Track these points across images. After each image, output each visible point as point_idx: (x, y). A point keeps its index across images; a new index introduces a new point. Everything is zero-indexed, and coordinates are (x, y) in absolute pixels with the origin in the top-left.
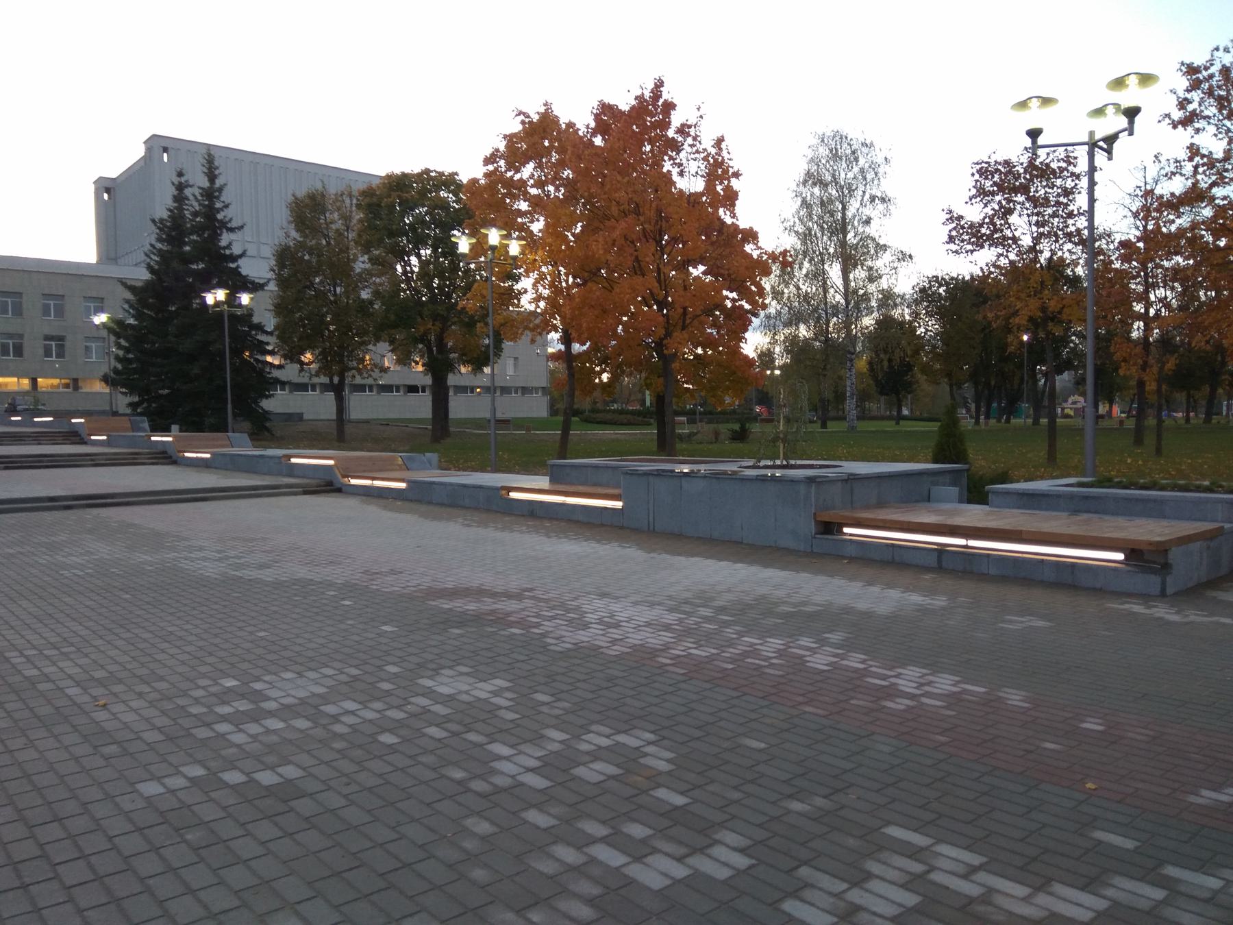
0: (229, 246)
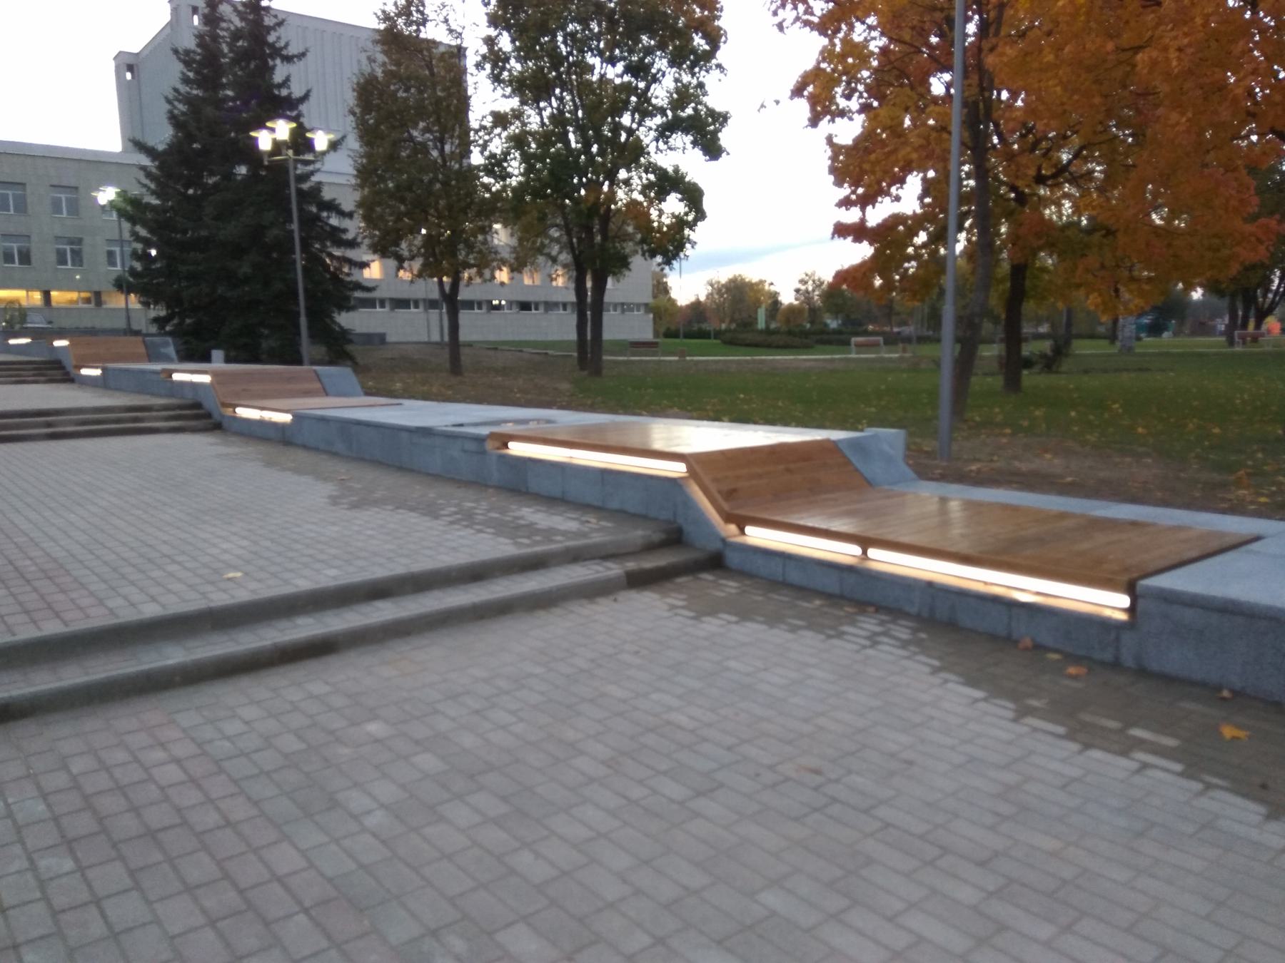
0: (286, 83)
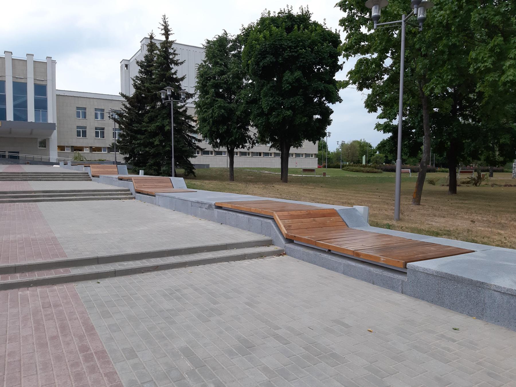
0: (175, 73)
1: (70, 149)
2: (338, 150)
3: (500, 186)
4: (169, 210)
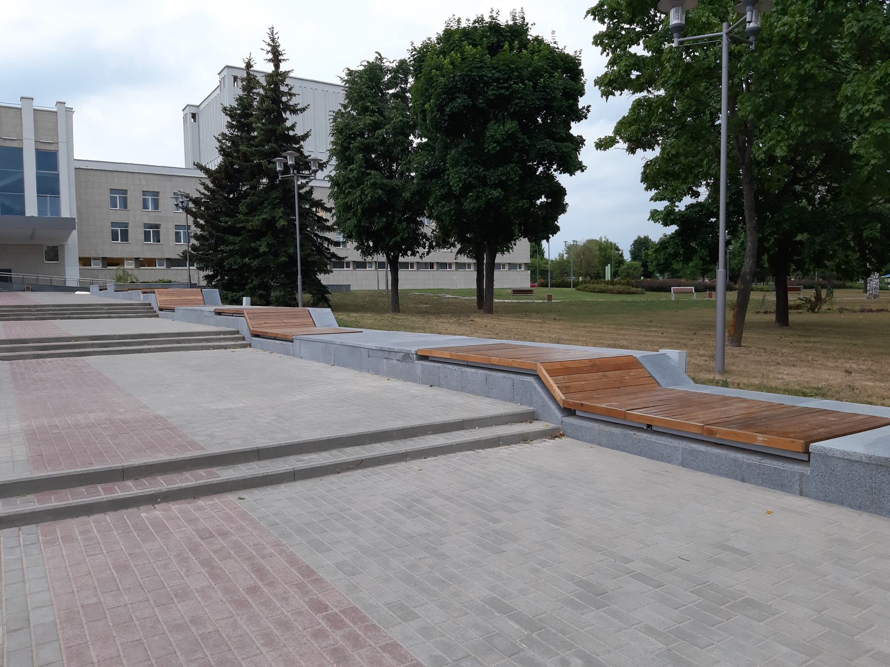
0: (293, 128)
1: (100, 262)
2: (561, 256)
3: (854, 312)
4: (323, 365)
